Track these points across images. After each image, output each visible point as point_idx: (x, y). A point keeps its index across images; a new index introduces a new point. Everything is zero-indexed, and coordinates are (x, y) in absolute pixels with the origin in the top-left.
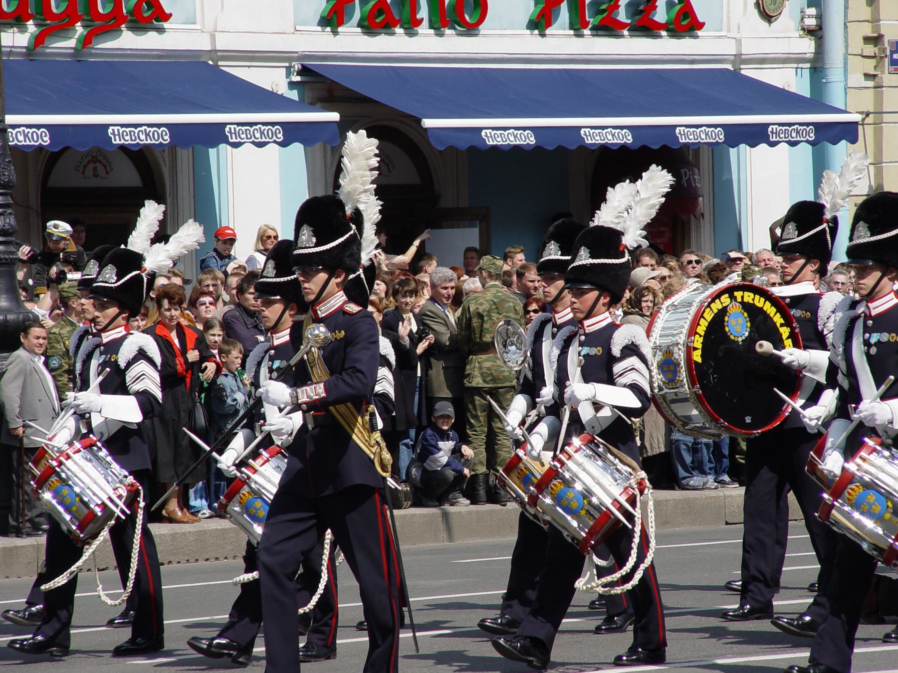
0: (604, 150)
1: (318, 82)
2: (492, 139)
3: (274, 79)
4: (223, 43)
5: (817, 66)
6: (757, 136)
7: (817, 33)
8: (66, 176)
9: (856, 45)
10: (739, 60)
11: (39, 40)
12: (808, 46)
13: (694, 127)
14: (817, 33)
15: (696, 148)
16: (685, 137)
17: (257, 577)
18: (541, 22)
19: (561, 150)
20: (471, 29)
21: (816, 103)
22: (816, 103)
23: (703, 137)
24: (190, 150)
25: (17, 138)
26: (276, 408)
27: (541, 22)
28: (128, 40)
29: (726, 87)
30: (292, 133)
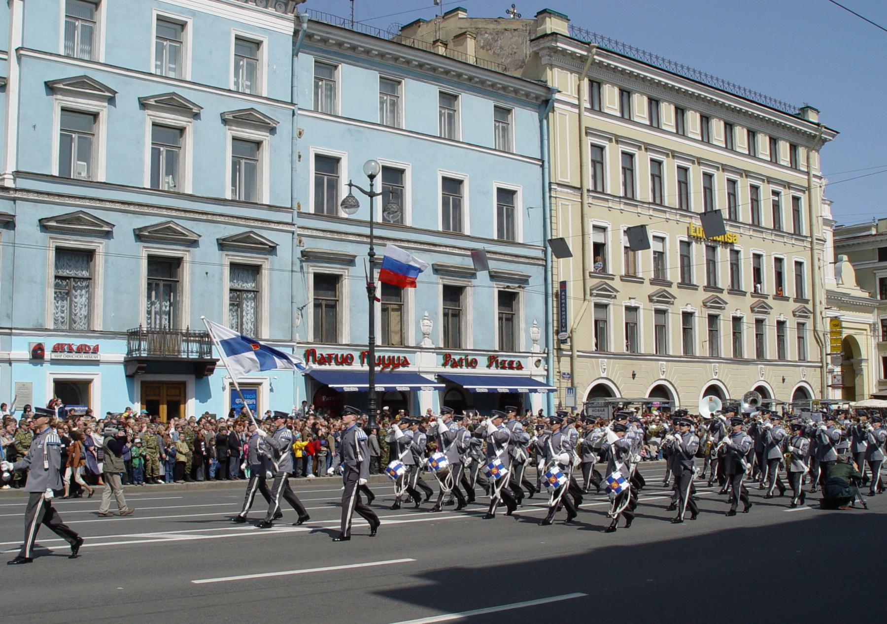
0: (503, 393)
1: (441, 378)
2: (346, 390)
3: (431, 377)
4: (421, 370)
5: (548, 377)
6: (535, 391)
7: (547, 370)
8: (386, 397)
9: (556, 373)
10: (531, 375)
11: (383, 369)
12: (545, 373)
13: (522, 389)
14: (547, 370)
15: (522, 393)
16: (520, 391)
17: (379, 270)
18: (489, 366)
19: (494, 393)
20: (474, 367)
21: (547, 385)
22: (547, 385)
23: (524, 391)
24: (488, 255)
25: (377, 389)
26: (299, 141)
27: (489, 366)
28: (401, 369)
29: (528, 381)
30: (436, 388)
